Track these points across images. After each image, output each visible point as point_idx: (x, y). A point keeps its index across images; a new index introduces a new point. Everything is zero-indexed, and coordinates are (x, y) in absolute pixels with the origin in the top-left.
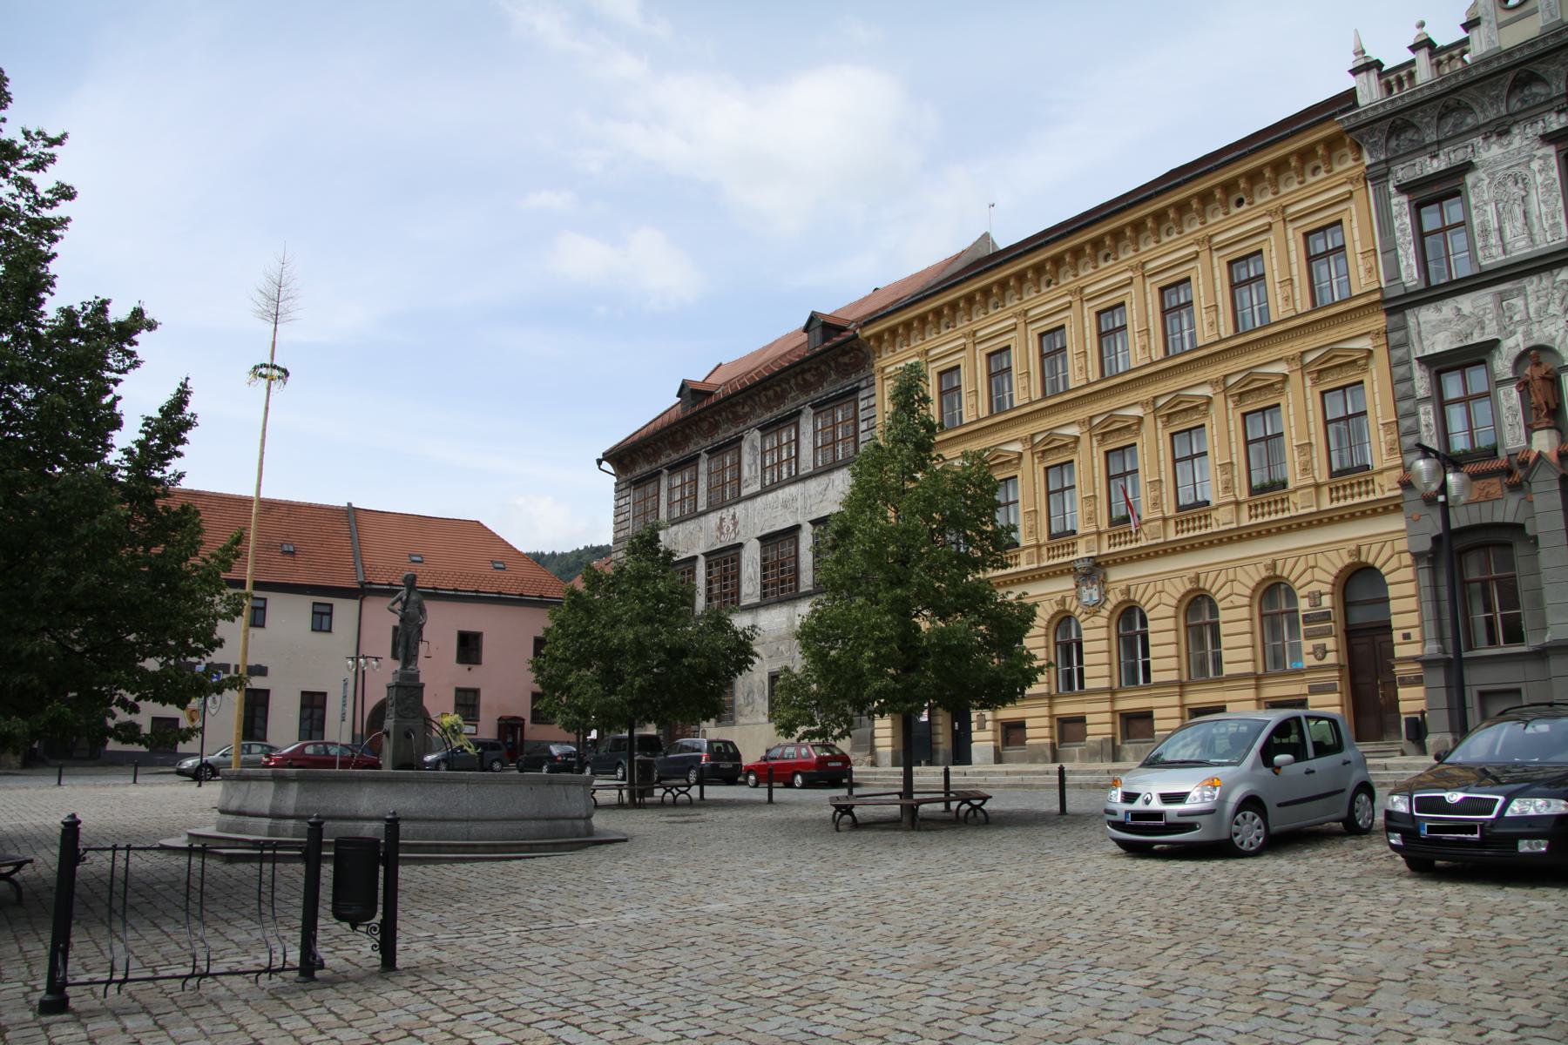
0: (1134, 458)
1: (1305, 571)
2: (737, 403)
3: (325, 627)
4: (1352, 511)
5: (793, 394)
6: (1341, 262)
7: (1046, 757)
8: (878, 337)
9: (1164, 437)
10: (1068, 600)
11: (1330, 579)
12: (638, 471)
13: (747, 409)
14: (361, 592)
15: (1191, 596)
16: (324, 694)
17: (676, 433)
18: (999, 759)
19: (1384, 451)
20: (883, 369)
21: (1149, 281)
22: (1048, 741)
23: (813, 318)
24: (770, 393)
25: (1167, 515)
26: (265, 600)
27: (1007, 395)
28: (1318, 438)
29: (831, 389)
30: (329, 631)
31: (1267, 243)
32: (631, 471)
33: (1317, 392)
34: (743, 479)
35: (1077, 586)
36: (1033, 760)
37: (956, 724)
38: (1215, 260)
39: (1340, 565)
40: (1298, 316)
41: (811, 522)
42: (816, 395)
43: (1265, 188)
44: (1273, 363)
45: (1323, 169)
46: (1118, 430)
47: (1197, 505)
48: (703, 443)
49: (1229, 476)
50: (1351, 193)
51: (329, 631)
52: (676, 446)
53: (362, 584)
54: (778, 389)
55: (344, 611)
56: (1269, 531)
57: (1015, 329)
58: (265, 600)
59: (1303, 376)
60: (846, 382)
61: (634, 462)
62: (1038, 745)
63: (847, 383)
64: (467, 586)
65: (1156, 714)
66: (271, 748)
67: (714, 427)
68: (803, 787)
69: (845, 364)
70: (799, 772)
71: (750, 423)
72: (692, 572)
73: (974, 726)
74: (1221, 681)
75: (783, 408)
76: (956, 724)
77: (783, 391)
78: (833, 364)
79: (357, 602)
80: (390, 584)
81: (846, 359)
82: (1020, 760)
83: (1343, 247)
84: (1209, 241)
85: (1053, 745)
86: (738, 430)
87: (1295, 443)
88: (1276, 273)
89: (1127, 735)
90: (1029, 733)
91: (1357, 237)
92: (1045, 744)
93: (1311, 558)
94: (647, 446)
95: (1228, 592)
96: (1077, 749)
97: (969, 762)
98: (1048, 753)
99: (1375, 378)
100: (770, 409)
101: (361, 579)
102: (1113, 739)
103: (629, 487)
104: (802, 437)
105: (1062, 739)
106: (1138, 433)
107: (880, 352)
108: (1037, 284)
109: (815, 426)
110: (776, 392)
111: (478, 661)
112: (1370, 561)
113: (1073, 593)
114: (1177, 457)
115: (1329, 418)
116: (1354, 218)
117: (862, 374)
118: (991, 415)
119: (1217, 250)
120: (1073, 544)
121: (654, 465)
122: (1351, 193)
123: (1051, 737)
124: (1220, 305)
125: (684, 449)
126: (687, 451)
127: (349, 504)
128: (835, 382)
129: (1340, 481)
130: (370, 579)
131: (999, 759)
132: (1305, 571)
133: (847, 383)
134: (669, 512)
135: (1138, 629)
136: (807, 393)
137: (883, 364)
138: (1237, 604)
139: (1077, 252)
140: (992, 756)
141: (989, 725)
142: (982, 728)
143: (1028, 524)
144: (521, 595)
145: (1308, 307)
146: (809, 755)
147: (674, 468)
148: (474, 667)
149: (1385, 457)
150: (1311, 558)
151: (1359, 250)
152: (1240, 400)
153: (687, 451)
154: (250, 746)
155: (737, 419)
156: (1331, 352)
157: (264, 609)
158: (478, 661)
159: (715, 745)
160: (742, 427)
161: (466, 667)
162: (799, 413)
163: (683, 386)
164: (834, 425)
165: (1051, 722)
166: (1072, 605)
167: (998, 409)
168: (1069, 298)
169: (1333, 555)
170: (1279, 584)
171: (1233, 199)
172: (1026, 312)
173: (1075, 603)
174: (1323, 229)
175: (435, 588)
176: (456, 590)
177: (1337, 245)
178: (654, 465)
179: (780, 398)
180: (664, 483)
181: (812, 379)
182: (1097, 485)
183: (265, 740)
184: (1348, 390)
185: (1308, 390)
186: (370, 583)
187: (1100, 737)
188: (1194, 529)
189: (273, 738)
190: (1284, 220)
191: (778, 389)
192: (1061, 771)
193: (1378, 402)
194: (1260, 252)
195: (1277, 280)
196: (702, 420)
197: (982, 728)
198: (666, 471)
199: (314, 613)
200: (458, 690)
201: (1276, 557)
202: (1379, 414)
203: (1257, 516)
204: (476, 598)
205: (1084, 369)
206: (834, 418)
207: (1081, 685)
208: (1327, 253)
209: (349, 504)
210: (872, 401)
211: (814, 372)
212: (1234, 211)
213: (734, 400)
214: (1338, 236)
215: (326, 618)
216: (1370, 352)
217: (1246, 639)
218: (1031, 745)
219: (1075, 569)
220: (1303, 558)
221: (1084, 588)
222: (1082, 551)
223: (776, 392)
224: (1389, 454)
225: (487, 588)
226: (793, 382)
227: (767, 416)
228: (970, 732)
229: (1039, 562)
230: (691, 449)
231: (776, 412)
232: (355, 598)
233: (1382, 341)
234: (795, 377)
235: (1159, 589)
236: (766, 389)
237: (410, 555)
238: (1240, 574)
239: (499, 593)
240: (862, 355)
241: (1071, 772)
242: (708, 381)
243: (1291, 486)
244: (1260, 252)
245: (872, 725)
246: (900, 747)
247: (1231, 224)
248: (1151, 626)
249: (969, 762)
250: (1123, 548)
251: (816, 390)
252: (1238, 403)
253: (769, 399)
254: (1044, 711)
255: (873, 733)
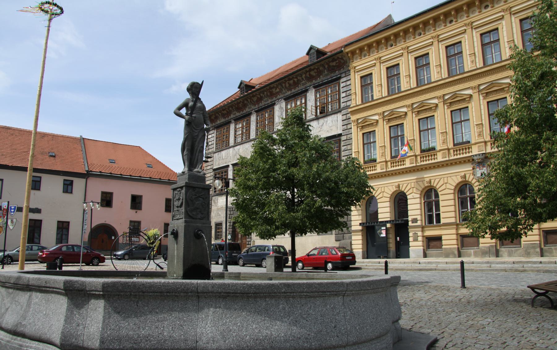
0: (374, 136)
1: (443, 184)
2: (274, 87)
3: (69, 191)
4: (426, 167)
5: (303, 82)
6: (498, 46)
7: (455, 255)
8: (353, 53)
9: (448, 112)
10: (467, 176)
11: (389, 196)
12: (218, 122)
13: (278, 90)
14: (87, 175)
15: (464, 183)
16: (68, 223)
17: (240, 103)
18: (425, 256)
19: (476, 136)
20: (355, 67)
21: (410, 55)
22: (456, 246)
23: (311, 48)
24: (291, 82)
25: (486, 140)
26: (41, 177)
27: (370, 95)
28: (486, 122)
29: (324, 78)
30: (71, 193)
31: (431, 50)
32: (215, 123)
33: (449, 111)
34: (275, 123)
35: (473, 169)
36: (447, 256)
37: (398, 238)
38: (410, 56)
39: (393, 191)
40: (442, 79)
41: (232, 164)
42: (316, 82)
43: (383, 47)
44: (432, 98)
45: (490, 6)
46: (396, 117)
47: (463, 143)
48: (253, 107)
49: (481, 130)
50: (503, 16)
51: (71, 193)
52: (239, 109)
53: (87, 171)
54: (296, 80)
55: (79, 184)
56: (375, 177)
57: (402, 55)
58: (41, 177)
59: (479, 95)
60: (333, 75)
61: (216, 118)
62: (450, 248)
63: (334, 75)
64: (136, 174)
65: (443, 237)
66: (44, 248)
67: (260, 99)
68: (333, 269)
69: (333, 66)
70: (330, 262)
71: (278, 97)
72: (227, 172)
73: (411, 239)
74: (440, 226)
75: (297, 89)
76: (398, 238)
77: (298, 80)
78: (326, 66)
79: (84, 180)
80: (100, 172)
81: (334, 64)
82: (438, 256)
83: (461, 52)
84: (471, 25)
85: (458, 248)
86: (272, 100)
87: (475, 123)
88: (404, 72)
89: (546, 243)
90: (444, 242)
91: (467, 48)
92: (454, 248)
93: (446, 179)
94: (224, 110)
95: (411, 192)
96: (472, 251)
97: (408, 256)
98: (456, 252)
99: (473, 106)
100: (290, 89)
101: (87, 169)
102: (496, 246)
103: (214, 129)
104: (308, 102)
105: (463, 246)
106: (469, 102)
107: (353, 59)
108: (414, 35)
109: (316, 96)
110: (294, 81)
111: (140, 208)
112: (403, 190)
113: (471, 172)
114: (453, 122)
115: (421, 129)
116: (467, 41)
117: (342, 71)
118: (389, 95)
119: (475, 29)
120: (375, 166)
121: (227, 119)
122: (465, 30)
123: (457, 245)
124: (442, 65)
125: (243, 111)
126: (245, 112)
127: (81, 136)
128: (327, 75)
129: (426, 154)
130: (91, 169)
131: (425, 256)
132: (443, 184)
133: (334, 75)
134: (235, 140)
135: (468, 195)
136: (311, 81)
137: (354, 65)
138: (415, 197)
139: (378, 43)
140: (422, 254)
141: (420, 239)
142: (416, 240)
143: (381, 152)
144: (160, 179)
145: (482, 65)
146: (337, 254)
147: (237, 120)
148: (139, 211)
149: (476, 138)
150: (446, 179)
151: (468, 53)
152: (486, 96)
153: (245, 112)
154: (32, 246)
155: (272, 95)
156: (455, 95)
157: (40, 182)
158: (140, 208)
159: (274, 248)
160: (274, 99)
161: (135, 211)
162: (306, 91)
163: (241, 83)
164: (327, 95)
165: (457, 237)
166: (470, 178)
167: (392, 92)
168: (402, 51)
169: (454, 178)
170: (466, 185)
171: (449, 20)
172: (380, 58)
173: (472, 177)
174: (489, 32)
175: (121, 175)
176: (130, 176)
177: (459, 52)
178: (227, 119)
179: (296, 84)
180: (232, 126)
181: (314, 74)
182: (483, 118)
183: (39, 244)
184: (429, 119)
185: (481, 101)
186: (91, 171)
187: (488, 245)
188: (426, 161)
189: (43, 243)
190: (472, 28)
191: (296, 80)
192: (462, 263)
193: (474, 115)
194: (460, 42)
195: (435, 65)
196: (254, 96)
197: (416, 240)
198: (233, 121)
199: (64, 184)
200: (131, 222)
201: (466, 173)
202: (475, 120)
203: (457, 155)
204: (140, 180)
205: (440, 72)
206: (327, 92)
207: (438, 221)
208: (455, 55)
209: (81, 136)
210: (348, 83)
211: (315, 71)
212: (448, 25)
213: (272, 86)
214: (459, 48)
215: (70, 187)
216: (406, 113)
217: (452, 208)
218: (445, 248)
219: (473, 160)
220: (380, 188)
221: (478, 169)
222: (475, 151)
223: (294, 81)
224: (443, 144)
225: (145, 175)
226: (304, 76)
227: (289, 93)
228: (408, 242)
229: (449, 157)
230: (247, 110)
231: (293, 91)
232: (84, 178)
233: (441, 100)
234: (305, 73)
235: (383, 191)
236: (290, 80)
237: (109, 160)
238: (386, 189)
239: (150, 178)
240: (342, 61)
241: (467, 263)
242: (251, 82)
243: (378, 161)
244: (460, 42)
245: (351, 238)
246: (365, 249)
247: (387, 53)
248: (441, 198)
249: (408, 256)
250: (397, 168)
251: (316, 79)
252: (387, 123)
253: (290, 85)
254: (454, 231)
255: (351, 242)
